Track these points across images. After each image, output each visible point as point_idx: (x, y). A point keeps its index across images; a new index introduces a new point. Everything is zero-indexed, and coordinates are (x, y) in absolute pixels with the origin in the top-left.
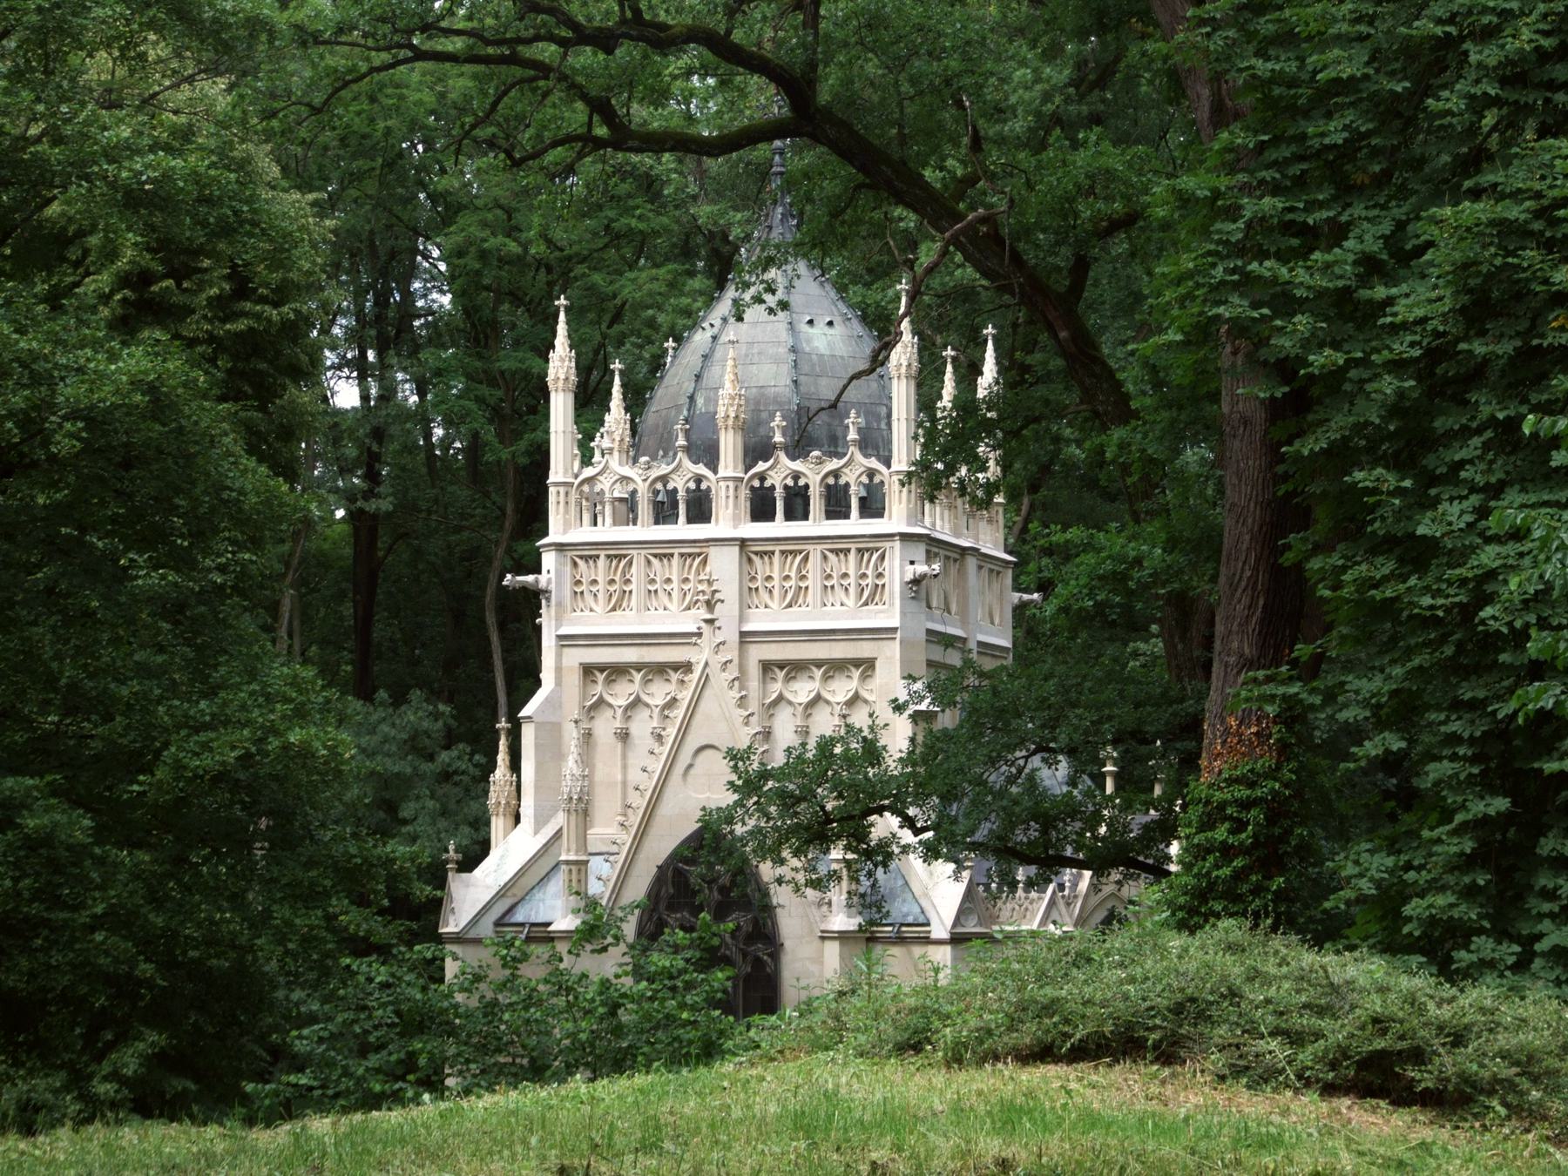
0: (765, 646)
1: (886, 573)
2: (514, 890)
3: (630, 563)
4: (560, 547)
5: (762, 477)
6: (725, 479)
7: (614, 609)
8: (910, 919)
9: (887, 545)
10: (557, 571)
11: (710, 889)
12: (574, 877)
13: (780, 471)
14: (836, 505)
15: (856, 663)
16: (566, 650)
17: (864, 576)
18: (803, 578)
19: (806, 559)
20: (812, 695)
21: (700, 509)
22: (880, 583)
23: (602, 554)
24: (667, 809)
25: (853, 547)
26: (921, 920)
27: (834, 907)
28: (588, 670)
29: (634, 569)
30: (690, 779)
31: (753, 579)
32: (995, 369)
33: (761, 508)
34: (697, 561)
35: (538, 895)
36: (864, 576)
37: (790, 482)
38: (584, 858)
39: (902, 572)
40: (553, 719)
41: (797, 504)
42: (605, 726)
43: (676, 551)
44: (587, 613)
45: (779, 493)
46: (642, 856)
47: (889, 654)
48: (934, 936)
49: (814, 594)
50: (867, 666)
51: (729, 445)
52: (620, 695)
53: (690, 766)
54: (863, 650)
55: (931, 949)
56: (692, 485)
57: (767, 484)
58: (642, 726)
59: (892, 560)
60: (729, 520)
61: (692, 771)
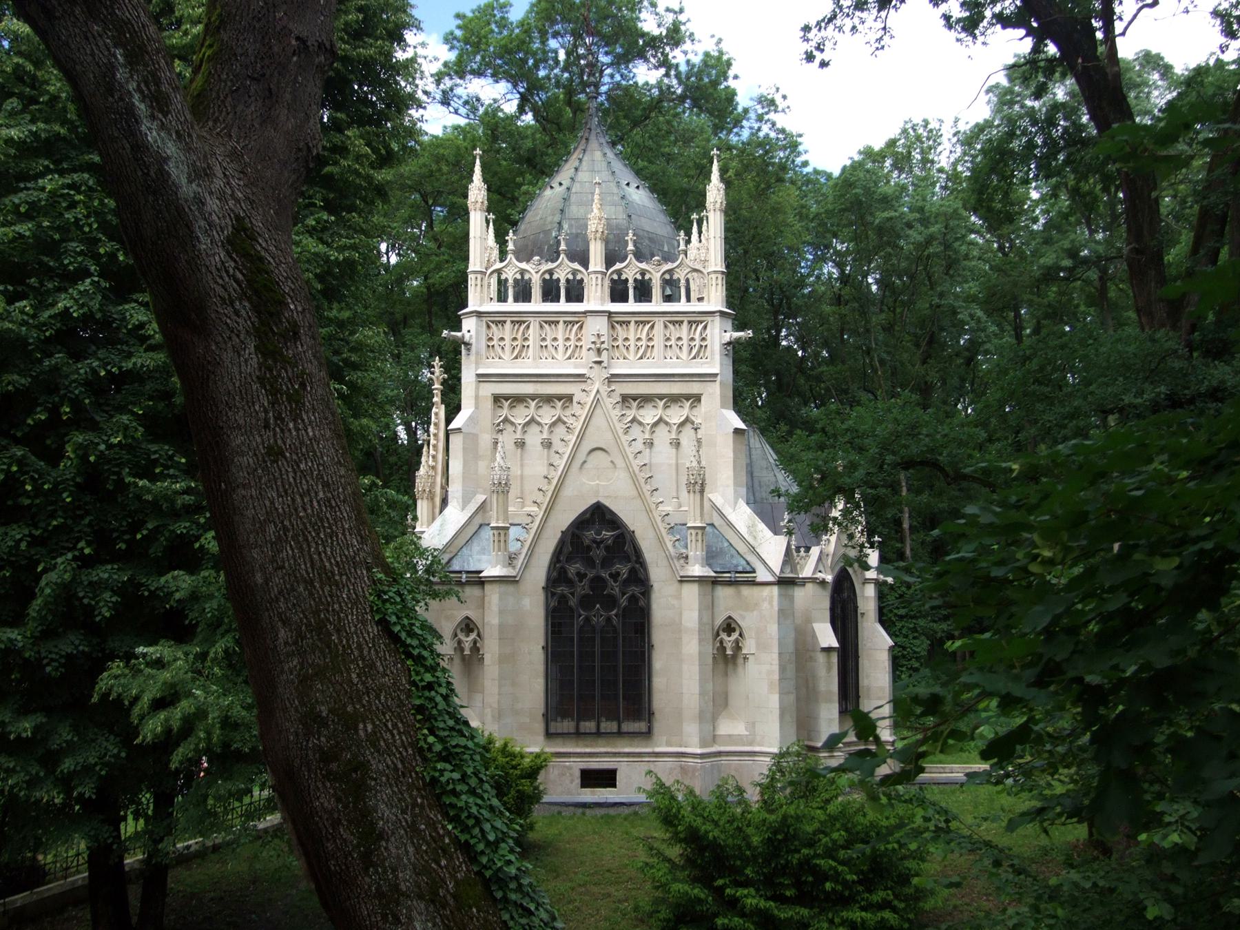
1: (708, 338)
3: (528, 327)
4: (479, 314)
5: (619, 272)
6: (595, 272)
8: (740, 569)
9: (710, 319)
12: (502, 538)
13: (631, 270)
14: (550, 292)
15: (687, 397)
17: (692, 339)
18: (526, 339)
21: (576, 292)
22: (651, 344)
23: (509, 320)
24: (568, 492)
25: (686, 320)
26: (748, 569)
27: (691, 560)
28: (497, 399)
29: (531, 331)
31: (615, 339)
32: (484, 193)
33: (618, 292)
36: (692, 339)
37: (571, 277)
39: (721, 338)
40: (474, 431)
41: (644, 292)
42: (508, 438)
43: (561, 320)
45: (631, 284)
46: (551, 523)
48: (758, 580)
49: (658, 351)
50: (697, 399)
51: (596, 253)
52: (520, 415)
54: (694, 388)
55: (755, 590)
56: (518, 276)
57: (555, 277)
59: (712, 329)
60: (596, 298)
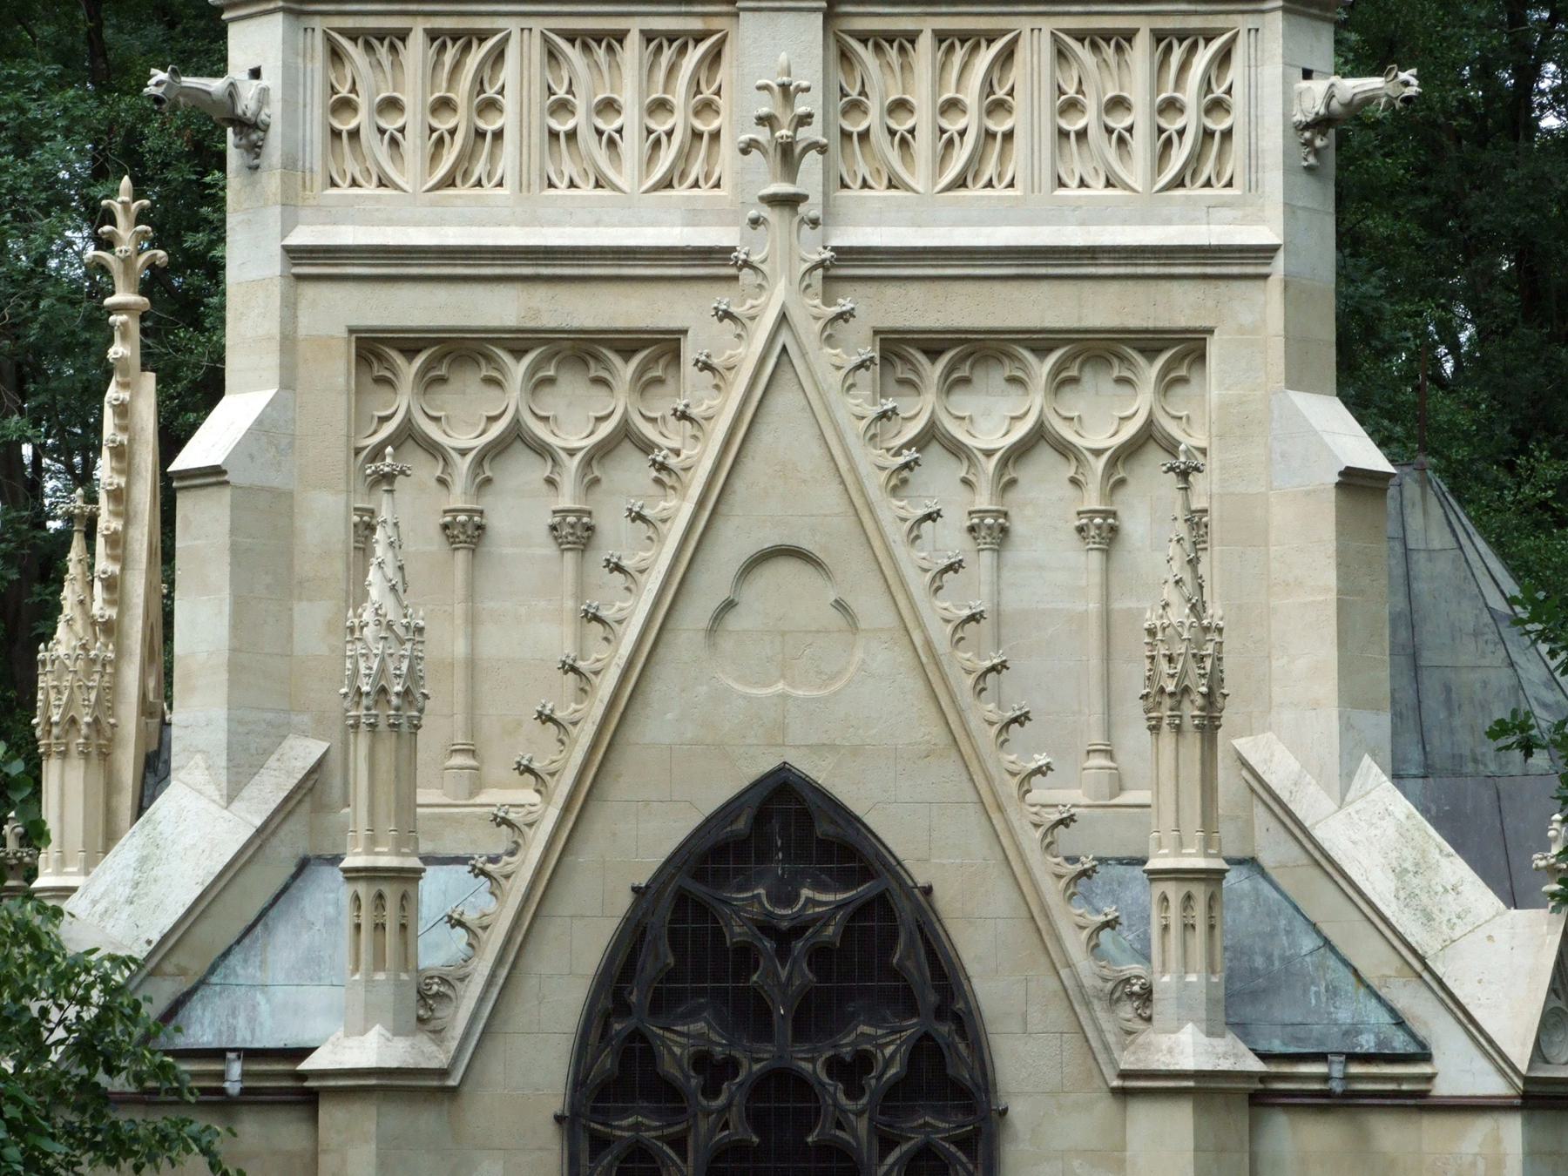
0: (891, 290)
1: (1238, 100)
2: (180, 958)
3: (498, 56)
7: (449, 182)
8: (1367, 1043)
10: (287, 67)
11: (783, 953)
15: (1150, 342)
16: (309, 291)
19: (1007, 56)
20: (1022, 430)
24: (662, 723)
26: (1400, 1043)
27: (1162, 1007)
28: (372, 350)
29: (509, 72)
30: (727, 644)
31: (855, 107)
34: (695, 55)
35: (241, 969)
36: (1171, 106)
38: (414, 862)
39: (1288, 101)
40: (276, 480)
44: (370, 189)
46: (587, 856)
47: (1247, 318)
48: (1443, 1088)
50: (1185, 350)
52: (466, 418)
53: (729, 605)
54: (1176, 306)
58: (522, 509)
59: (1252, 65)
61: (733, 622)
